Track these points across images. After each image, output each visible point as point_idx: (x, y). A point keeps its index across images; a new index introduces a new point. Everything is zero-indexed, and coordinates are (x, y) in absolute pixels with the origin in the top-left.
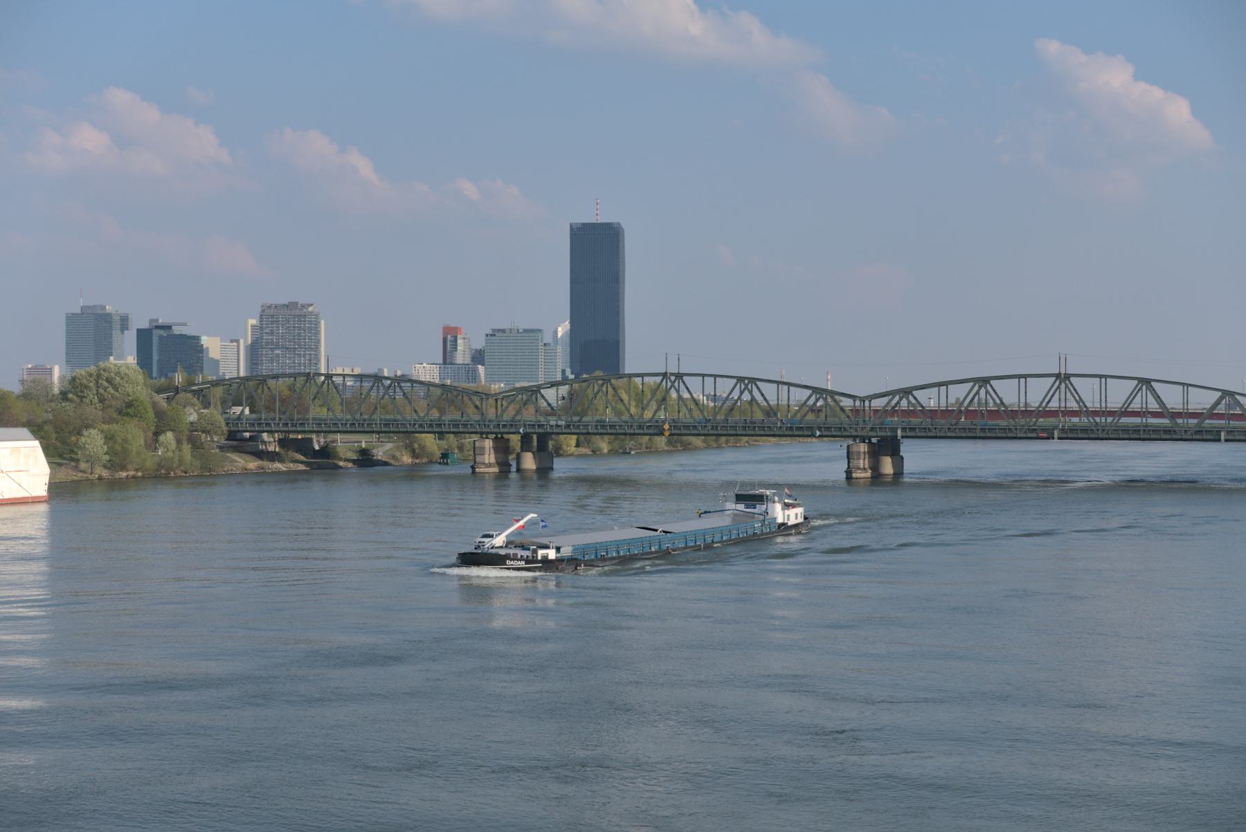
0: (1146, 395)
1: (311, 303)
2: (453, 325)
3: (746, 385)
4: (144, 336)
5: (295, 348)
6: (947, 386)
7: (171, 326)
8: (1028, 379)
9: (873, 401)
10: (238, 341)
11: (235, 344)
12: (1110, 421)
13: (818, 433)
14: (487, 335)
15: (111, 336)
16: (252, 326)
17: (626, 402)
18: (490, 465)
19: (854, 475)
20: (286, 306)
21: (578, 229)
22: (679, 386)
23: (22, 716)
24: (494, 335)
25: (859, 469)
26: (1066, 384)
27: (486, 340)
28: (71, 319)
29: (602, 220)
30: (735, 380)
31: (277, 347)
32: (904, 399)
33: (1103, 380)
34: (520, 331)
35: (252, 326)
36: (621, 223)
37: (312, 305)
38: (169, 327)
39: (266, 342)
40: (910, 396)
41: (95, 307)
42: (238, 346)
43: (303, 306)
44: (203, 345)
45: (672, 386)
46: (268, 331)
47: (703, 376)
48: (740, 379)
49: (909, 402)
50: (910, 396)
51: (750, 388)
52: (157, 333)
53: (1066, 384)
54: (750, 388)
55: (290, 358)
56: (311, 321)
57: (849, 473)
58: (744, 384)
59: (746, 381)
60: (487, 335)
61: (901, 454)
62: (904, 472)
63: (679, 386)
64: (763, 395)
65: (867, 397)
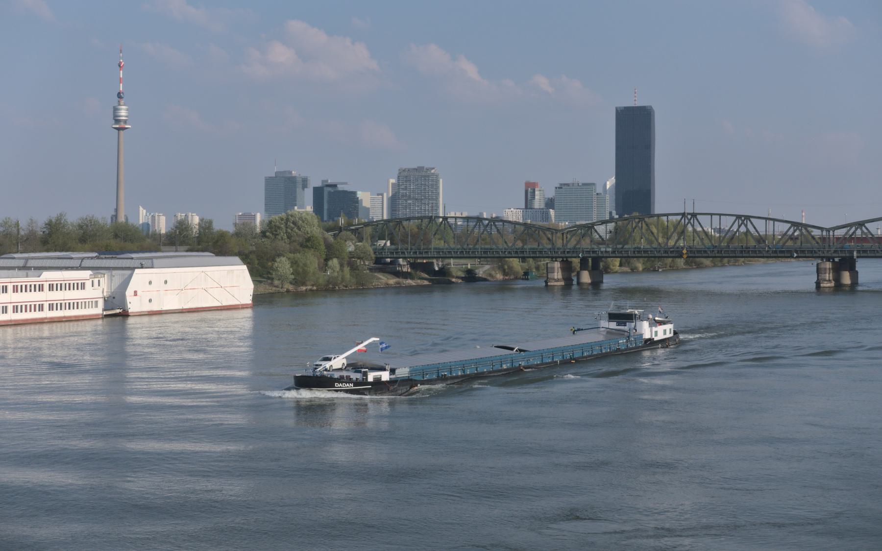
1: (433, 167)
2: (532, 181)
4: (318, 192)
5: (422, 199)
8: (722, 217)
10: (382, 195)
11: (380, 196)
13: (795, 255)
14: (556, 188)
15: (295, 192)
16: (392, 184)
18: (558, 280)
19: (822, 285)
20: (416, 170)
21: (621, 110)
22: (694, 222)
24: (562, 188)
25: (826, 280)
27: (556, 191)
28: (269, 181)
29: (639, 104)
30: (789, 225)
31: (410, 198)
35: (392, 184)
37: (433, 168)
38: (334, 186)
39: (402, 195)
41: (285, 172)
42: (383, 198)
43: (427, 169)
46: (403, 187)
47: (711, 214)
48: (739, 217)
49: (863, 232)
52: (327, 190)
54: (692, 222)
55: (418, 206)
56: (433, 180)
57: (818, 284)
58: (741, 220)
59: (743, 218)
60: (556, 188)
61: (857, 269)
62: (604, 281)
63: (694, 222)
64: (755, 228)
65: (831, 229)
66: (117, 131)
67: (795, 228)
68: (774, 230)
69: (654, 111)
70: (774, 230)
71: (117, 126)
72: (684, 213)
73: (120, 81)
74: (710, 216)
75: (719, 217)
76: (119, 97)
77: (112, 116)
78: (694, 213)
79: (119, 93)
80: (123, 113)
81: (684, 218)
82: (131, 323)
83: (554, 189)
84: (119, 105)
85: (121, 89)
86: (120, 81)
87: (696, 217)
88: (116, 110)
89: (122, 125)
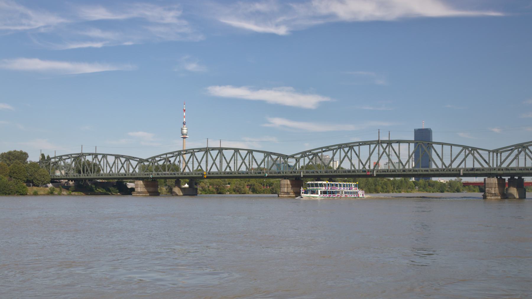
0: (481, 156)
7: (184, 195)
14: (385, 164)
21: (417, 131)
23: (168, 250)
26: (475, 157)
29: (424, 127)
30: (461, 148)
32: (523, 152)
33: (491, 153)
36: (431, 129)
37: (328, 156)
40: (527, 150)
48: (465, 147)
50: (527, 150)
53: (475, 157)
58: (469, 150)
59: (470, 149)
66: (183, 139)
68: (220, 142)
69: (432, 131)
70: (220, 142)
71: (182, 136)
74: (450, 146)
78: (389, 140)
79: (184, 122)
80: (185, 131)
81: (388, 146)
82: (392, 145)
83: (384, 165)
85: (184, 120)
87: (353, 149)
88: (182, 129)
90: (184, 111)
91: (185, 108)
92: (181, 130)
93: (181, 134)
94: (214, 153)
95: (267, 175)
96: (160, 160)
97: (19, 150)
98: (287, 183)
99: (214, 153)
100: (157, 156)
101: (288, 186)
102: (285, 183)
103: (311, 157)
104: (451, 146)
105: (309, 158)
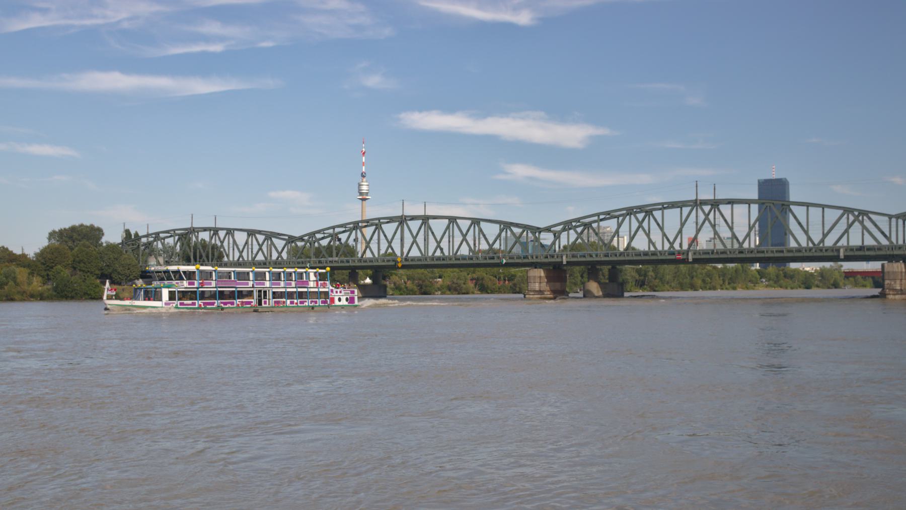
3: (856, 219)
6: (681, 208)
8: (810, 208)
9: (542, 233)
11: (251, 286)
12: (172, 239)
14: (707, 241)
17: (364, 241)
22: (715, 218)
26: (864, 227)
30: (841, 212)
33: (894, 220)
34: (726, 238)
37: (608, 227)
42: (250, 288)
44: (35, 254)
45: (640, 226)
48: (847, 211)
51: (646, 228)
53: (864, 227)
58: (854, 215)
59: (856, 213)
63: (715, 218)
67: (502, 226)
71: (361, 197)
72: (696, 200)
73: (363, 164)
74: (821, 209)
75: (821, 209)
76: (362, 176)
77: (357, 190)
78: (715, 199)
79: (362, 173)
80: (365, 188)
84: (362, 182)
86: (363, 164)
88: (360, 185)
89: (365, 197)
90: (364, 153)
91: (364, 149)
92: (359, 187)
93: (358, 194)
94: (415, 225)
95: (504, 261)
96: (323, 238)
97: (88, 224)
98: (539, 275)
99: (415, 225)
100: (319, 232)
101: (540, 279)
102: (536, 275)
103: (579, 230)
104: (823, 209)
105: (576, 232)
